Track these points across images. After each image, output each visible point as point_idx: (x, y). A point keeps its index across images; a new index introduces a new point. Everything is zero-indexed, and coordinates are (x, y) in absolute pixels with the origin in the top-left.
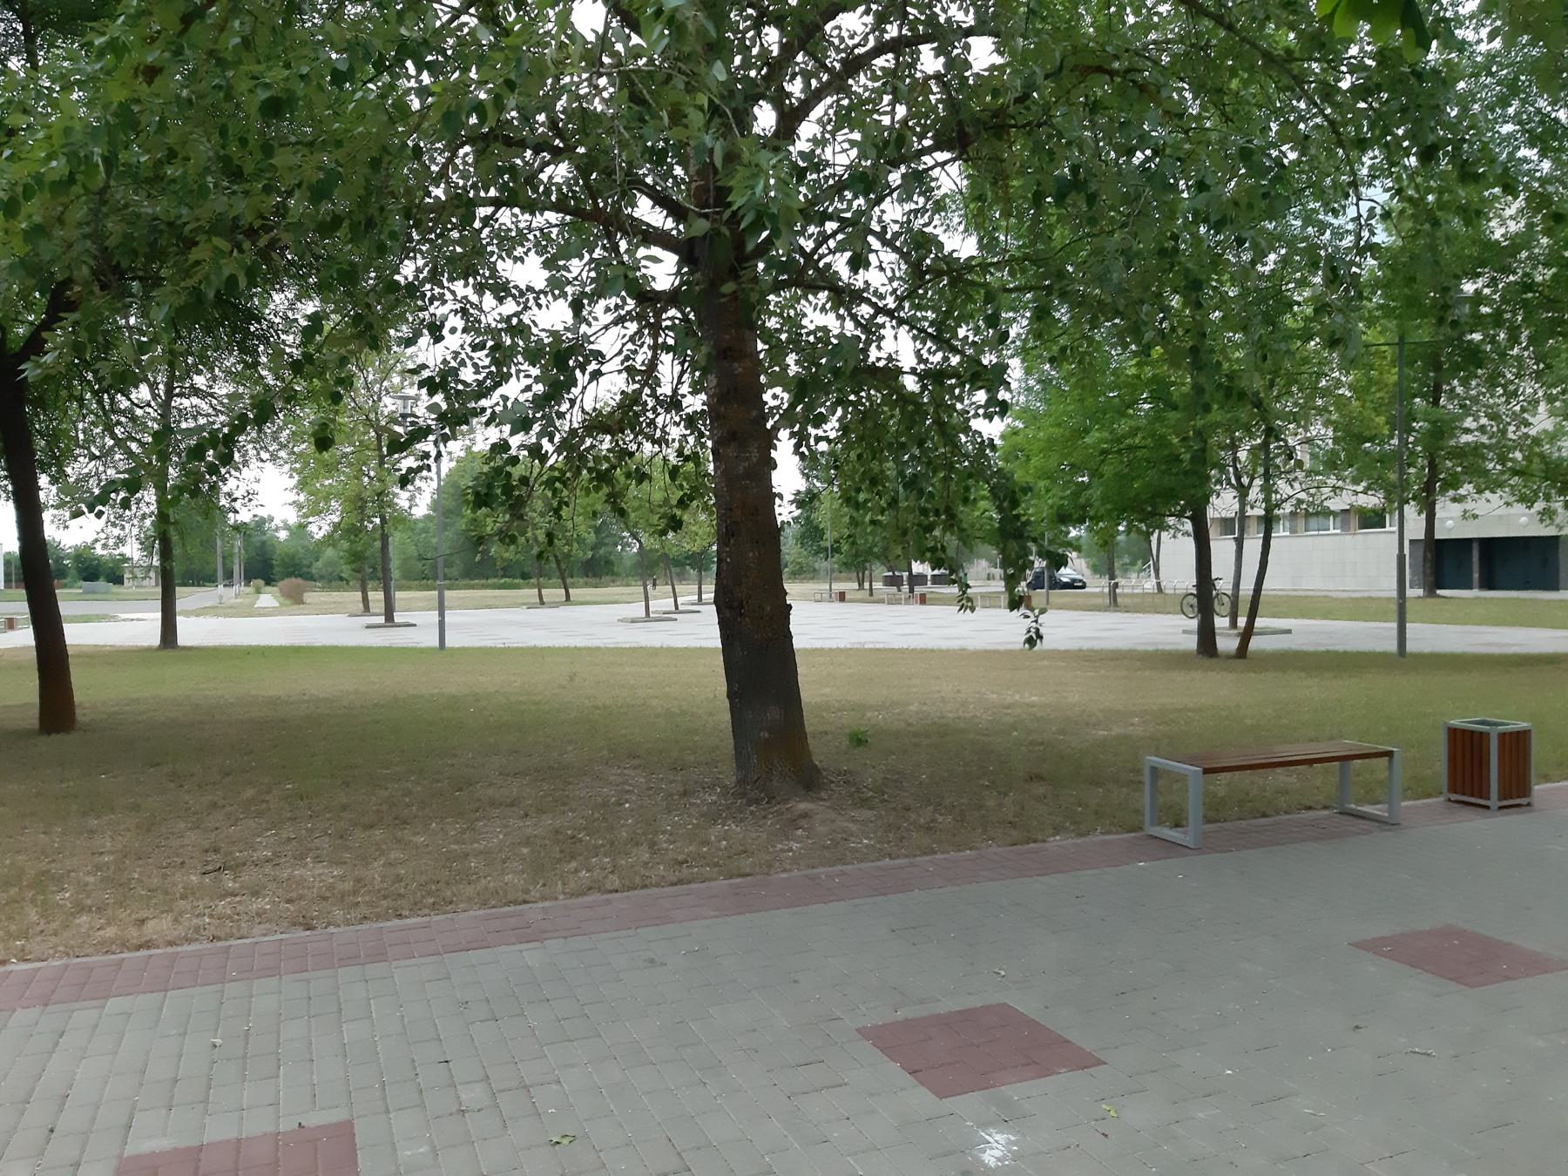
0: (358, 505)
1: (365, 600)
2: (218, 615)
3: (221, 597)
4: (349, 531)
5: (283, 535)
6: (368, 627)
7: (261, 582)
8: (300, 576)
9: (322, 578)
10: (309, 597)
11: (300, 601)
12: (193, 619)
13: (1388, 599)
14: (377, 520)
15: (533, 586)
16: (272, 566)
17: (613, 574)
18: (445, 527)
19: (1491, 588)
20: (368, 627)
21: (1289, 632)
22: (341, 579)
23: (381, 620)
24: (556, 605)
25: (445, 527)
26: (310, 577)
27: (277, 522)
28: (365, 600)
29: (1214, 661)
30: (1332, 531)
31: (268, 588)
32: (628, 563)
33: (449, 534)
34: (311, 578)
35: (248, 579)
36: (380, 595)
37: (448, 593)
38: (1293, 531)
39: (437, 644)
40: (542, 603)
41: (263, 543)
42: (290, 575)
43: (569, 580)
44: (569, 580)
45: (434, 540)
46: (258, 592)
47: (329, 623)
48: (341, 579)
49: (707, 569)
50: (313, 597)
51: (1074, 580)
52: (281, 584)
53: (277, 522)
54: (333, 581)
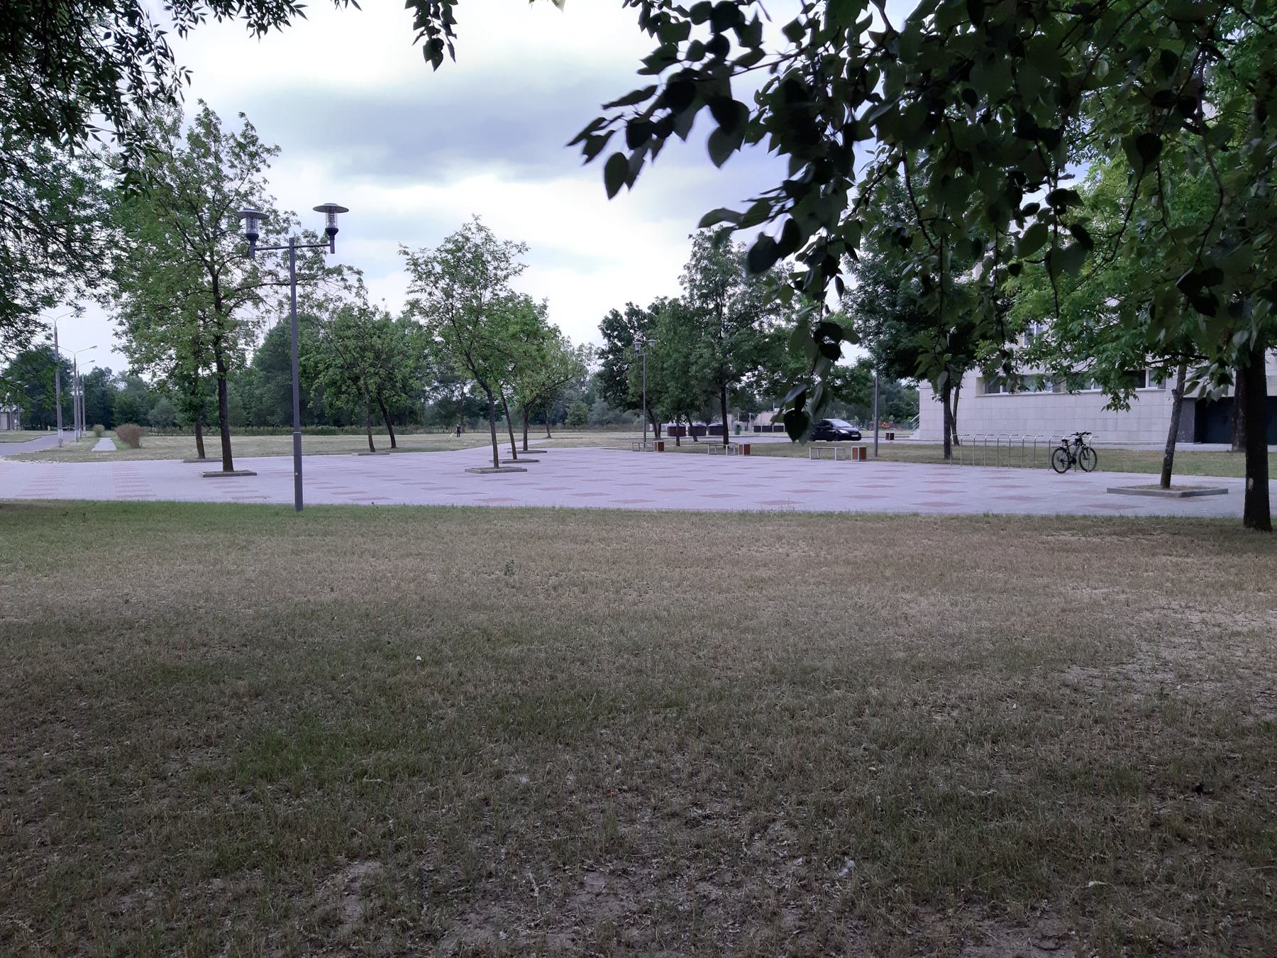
0: (196, 351)
1: (200, 446)
2: (53, 460)
3: (61, 441)
4: (183, 377)
5: (122, 386)
6: (207, 476)
7: (101, 427)
8: (136, 421)
9: (158, 423)
10: (144, 441)
11: (135, 444)
12: (28, 463)
13: (1157, 453)
14: (214, 367)
15: (484, 429)
16: (112, 413)
17: (417, 422)
18: (268, 380)
19: (1204, 442)
20: (207, 476)
21: (1225, 492)
22: (175, 425)
23: (219, 467)
24: (385, 452)
25: (268, 380)
26: (144, 422)
27: (115, 373)
28: (200, 446)
29: (1267, 535)
30: (1093, 390)
31: (108, 433)
32: (428, 414)
33: (271, 386)
34: (148, 423)
35: (90, 422)
36: (217, 440)
37: (305, 439)
38: (1056, 390)
39: (291, 499)
40: (373, 449)
41: (104, 393)
42: (129, 420)
43: (204, 429)
44: (204, 429)
45: (257, 392)
46: (99, 435)
47: (164, 472)
48: (175, 425)
49: (498, 419)
50: (152, 441)
51: (851, 433)
52: (118, 428)
53: (115, 373)
54: (168, 426)
